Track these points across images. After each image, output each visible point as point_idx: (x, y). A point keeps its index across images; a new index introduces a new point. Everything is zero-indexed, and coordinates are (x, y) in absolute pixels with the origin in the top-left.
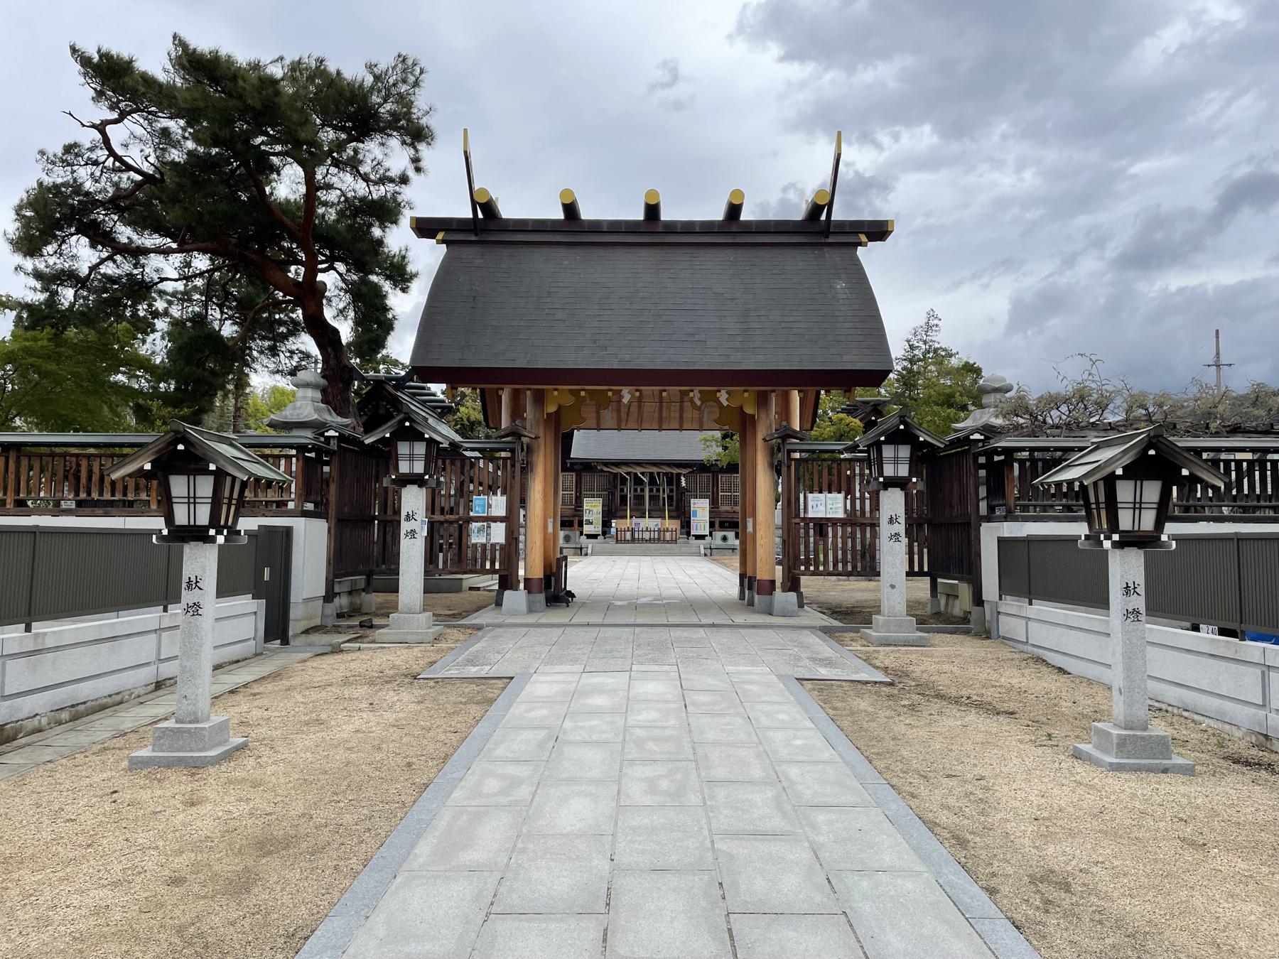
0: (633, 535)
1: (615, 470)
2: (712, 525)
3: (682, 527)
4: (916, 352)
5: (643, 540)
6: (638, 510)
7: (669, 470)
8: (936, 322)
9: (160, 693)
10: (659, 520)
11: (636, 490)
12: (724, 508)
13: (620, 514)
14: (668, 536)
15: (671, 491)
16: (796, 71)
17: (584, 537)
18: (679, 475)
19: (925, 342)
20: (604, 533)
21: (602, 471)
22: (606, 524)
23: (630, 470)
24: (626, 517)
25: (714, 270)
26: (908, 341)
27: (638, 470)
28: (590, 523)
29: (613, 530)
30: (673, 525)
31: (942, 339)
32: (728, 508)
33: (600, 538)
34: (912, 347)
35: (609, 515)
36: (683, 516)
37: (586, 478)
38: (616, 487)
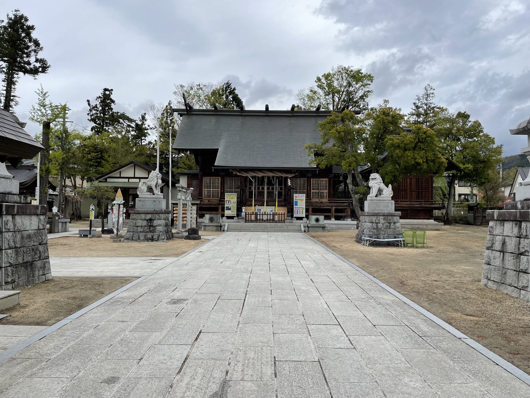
1: (245, 175)
2: (307, 210)
3: (288, 212)
4: (421, 109)
5: (263, 221)
7: (280, 174)
8: (432, 91)
10: (273, 207)
11: (258, 188)
12: (314, 200)
15: (281, 189)
16: (342, 26)
18: (286, 178)
19: (426, 105)
20: (238, 215)
21: (236, 176)
22: (239, 210)
23: (254, 174)
26: (415, 104)
27: (260, 175)
28: (229, 209)
29: (243, 214)
30: (283, 210)
31: (436, 102)
32: (317, 200)
33: (236, 218)
34: (418, 107)
35: (241, 204)
36: (288, 203)
37: (228, 181)
38: (246, 186)
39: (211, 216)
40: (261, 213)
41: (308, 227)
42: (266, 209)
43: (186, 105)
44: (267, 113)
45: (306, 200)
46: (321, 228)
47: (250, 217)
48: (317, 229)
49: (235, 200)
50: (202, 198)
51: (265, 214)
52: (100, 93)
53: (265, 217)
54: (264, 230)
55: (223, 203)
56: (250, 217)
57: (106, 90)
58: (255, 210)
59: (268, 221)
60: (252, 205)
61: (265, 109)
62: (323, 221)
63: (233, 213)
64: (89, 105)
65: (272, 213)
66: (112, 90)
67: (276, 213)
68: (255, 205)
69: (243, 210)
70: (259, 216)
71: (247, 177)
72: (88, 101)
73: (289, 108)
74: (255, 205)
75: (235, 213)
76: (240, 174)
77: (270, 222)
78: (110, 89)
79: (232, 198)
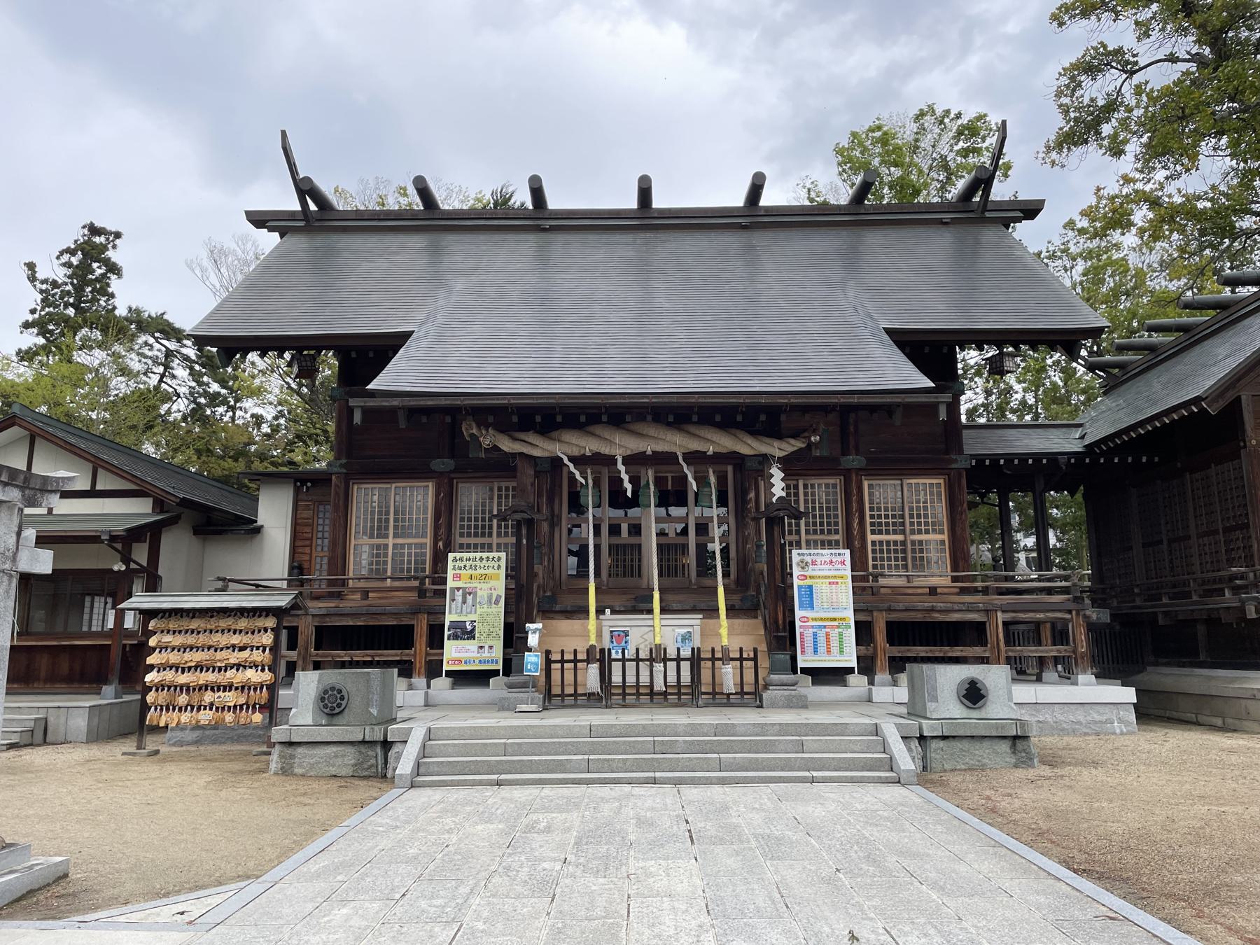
0: (605, 676)
1: (541, 447)
2: (863, 632)
6: (623, 591)
9: (37, 757)
10: (693, 622)
12: (892, 579)
13: (568, 602)
14: (728, 676)
17: (442, 683)
22: (514, 639)
23: (589, 445)
24: (583, 612)
25: (602, 268)
28: (464, 632)
29: (533, 661)
30: (728, 633)
35: (522, 604)
39: (333, 677)
41: (922, 738)
42: (666, 630)
43: (305, 189)
44: (645, 219)
45: (854, 578)
46: (1004, 747)
47: (569, 677)
48: (983, 752)
49: (499, 585)
50: (344, 583)
52: (73, 235)
53: (661, 677)
54: (656, 766)
55: (436, 601)
56: (569, 677)
57: (94, 230)
58: (599, 635)
60: (587, 612)
61: (632, 203)
62: (1010, 697)
63: (486, 654)
64: (32, 279)
65: (686, 653)
66: (118, 235)
67: (725, 650)
68: (600, 611)
69: (533, 640)
70: (616, 668)
71: (556, 462)
72: (31, 266)
73: (737, 199)
75: (498, 653)
76: (517, 447)
77: (679, 704)
78: (111, 227)
79: (484, 578)
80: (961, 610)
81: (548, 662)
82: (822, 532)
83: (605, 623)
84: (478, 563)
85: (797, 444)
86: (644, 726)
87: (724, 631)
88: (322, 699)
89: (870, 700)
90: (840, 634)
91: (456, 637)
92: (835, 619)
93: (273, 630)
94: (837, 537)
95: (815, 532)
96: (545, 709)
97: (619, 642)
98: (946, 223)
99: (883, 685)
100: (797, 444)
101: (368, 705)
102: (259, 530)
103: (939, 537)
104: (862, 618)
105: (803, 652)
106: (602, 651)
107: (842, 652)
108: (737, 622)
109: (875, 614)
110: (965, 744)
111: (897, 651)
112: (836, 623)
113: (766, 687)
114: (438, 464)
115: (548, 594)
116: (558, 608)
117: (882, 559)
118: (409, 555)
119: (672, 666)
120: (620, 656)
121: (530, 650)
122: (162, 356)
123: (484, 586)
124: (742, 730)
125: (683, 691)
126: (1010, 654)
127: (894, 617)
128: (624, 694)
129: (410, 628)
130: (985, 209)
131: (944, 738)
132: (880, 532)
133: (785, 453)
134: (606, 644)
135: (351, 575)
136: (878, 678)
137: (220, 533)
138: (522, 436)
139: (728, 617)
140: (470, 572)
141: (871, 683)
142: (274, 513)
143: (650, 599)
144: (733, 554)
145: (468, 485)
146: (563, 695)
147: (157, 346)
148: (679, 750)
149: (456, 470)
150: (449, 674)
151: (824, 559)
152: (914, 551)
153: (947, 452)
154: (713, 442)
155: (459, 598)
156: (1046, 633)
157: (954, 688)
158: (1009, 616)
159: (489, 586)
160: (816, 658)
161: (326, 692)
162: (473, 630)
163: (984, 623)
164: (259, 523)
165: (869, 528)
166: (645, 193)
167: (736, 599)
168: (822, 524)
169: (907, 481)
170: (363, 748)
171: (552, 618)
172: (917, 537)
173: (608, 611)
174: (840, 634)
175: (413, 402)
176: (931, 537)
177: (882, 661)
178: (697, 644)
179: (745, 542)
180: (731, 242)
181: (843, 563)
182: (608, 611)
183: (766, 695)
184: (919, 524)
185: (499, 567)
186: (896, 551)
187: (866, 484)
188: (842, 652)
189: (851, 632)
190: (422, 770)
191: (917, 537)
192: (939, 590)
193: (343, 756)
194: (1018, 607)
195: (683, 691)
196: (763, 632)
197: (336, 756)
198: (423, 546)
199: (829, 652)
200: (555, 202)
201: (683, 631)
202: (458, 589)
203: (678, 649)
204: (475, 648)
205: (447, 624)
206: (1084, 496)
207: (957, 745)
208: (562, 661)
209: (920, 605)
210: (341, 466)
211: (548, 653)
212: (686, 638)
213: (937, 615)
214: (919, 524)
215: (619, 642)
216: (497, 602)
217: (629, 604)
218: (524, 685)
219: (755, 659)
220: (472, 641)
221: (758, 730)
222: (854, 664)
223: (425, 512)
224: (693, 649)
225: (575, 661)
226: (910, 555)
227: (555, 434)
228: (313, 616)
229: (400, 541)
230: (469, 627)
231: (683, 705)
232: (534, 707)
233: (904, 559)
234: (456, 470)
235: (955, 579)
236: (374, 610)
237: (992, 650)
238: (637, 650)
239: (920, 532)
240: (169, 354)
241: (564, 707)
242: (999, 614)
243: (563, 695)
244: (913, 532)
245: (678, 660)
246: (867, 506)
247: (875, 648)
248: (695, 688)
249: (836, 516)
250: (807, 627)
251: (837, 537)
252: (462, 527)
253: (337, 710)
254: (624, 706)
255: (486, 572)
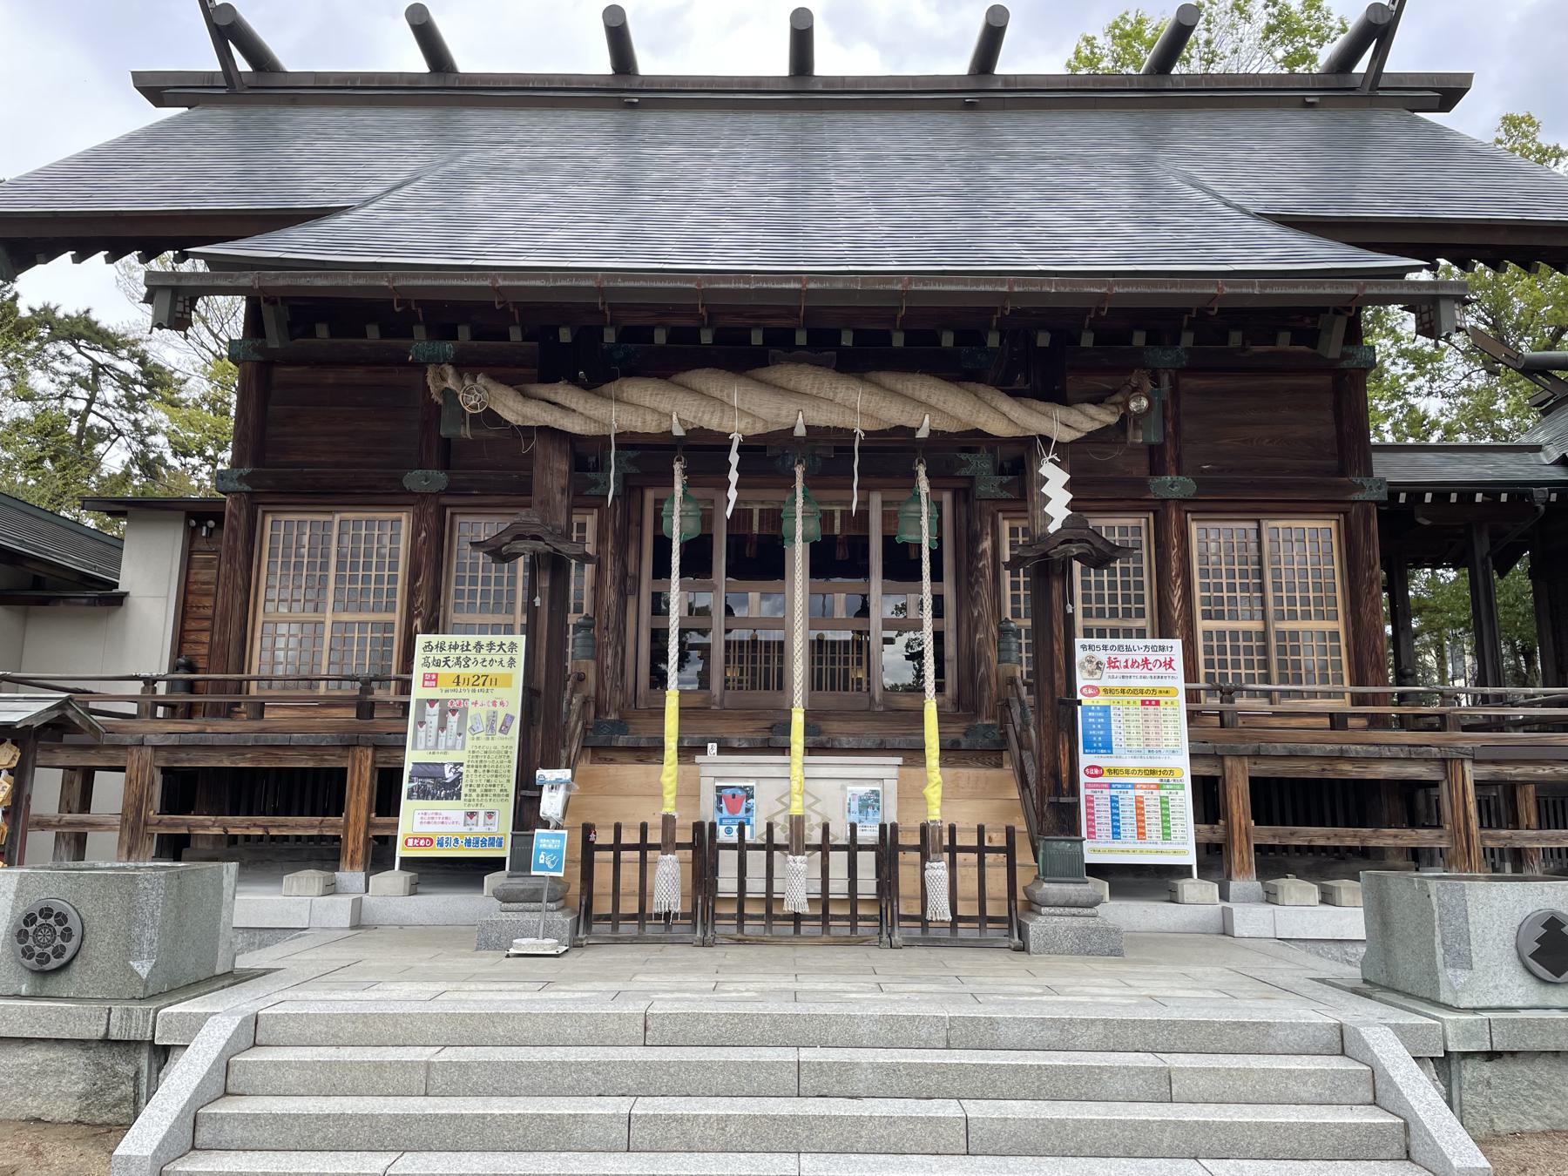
5: (768, 922)
10: (883, 771)
18: (1017, 460)
28: (440, 785)
29: (552, 849)
30: (941, 795)
36: (1024, 730)
40: (755, 834)
42: (819, 791)
43: (228, 31)
47: (630, 874)
50: (240, 687)
51: (797, 844)
56: (630, 874)
58: (688, 793)
59: (830, 921)
61: (779, 65)
63: (480, 828)
65: (869, 834)
68: (688, 752)
70: (727, 860)
73: (959, 65)
74: (688, 752)
75: (503, 825)
79: (482, 681)
80: (1389, 759)
81: (589, 848)
82: (1114, 613)
83: (705, 771)
84: (472, 654)
85: (1104, 417)
86: (776, 1021)
87: (934, 793)
88: (22, 935)
89: (1226, 930)
90: (1164, 801)
91: (422, 793)
92: (1153, 772)
93: (11, 772)
94: (1140, 623)
95: (1101, 614)
96: (576, 945)
97: (733, 810)
98: (1311, 105)
99: (1246, 899)
100: (1104, 417)
101: (128, 954)
102: (119, 600)
103: (1328, 626)
104: (1206, 770)
105: (414, 747)
106: (698, 827)
107: (1166, 836)
108: (968, 774)
109: (1228, 763)
110: (1541, 1071)
111: (1269, 835)
112: (1155, 780)
113: (1033, 906)
114: (415, 480)
115: (613, 717)
116: (622, 741)
117: (1223, 664)
118: (362, 640)
119: (839, 860)
120: (734, 838)
121: (546, 824)
122: (86, 373)
123: (479, 697)
124: (1013, 1034)
125: (861, 911)
126: (1489, 844)
127: (1265, 769)
128: (741, 917)
129: (338, 778)
130: (1375, 86)
131: (1492, 1055)
132: (1220, 616)
133: (1097, 426)
134: (707, 813)
135: (254, 673)
136: (1235, 886)
137: (45, 602)
138: (544, 390)
139: (944, 762)
140: (456, 670)
141: (1224, 896)
142: (150, 574)
143: (786, 729)
144: (950, 650)
145: (471, 519)
146: (615, 918)
147: (78, 358)
148: (860, 1088)
149: (448, 492)
150: (407, 863)
151: (1131, 656)
152: (1282, 650)
153: (1342, 472)
154: (930, 408)
155: (433, 713)
156: (1528, 806)
157: (1509, 936)
158: (1486, 771)
159: (490, 697)
160: (1117, 845)
161: (30, 919)
162: (457, 781)
163: (1435, 784)
164: (121, 589)
165: (1198, 609)
166: (802, 41)
167: (956, 730)
168: (1113, 599)
169: (1268, 525)
170: (105, 1057)
171: (612, 761)
172: (1287, 625)
173: (712, 748)
174: (1164, 801)
175: (282, 280)
176: (1314, 625)
177: (1243, 855)
178: (891, 817)
179: (974, 626)
180: (954, 125)
181: (1169, 664)
182: (712, 748)
183: (1036, 927)
184: (1292, 601)
185: (512, 662)
186: (1249, 650)
187: (1194, 527)
188: (1166, 836)
189: (1186, 796)
190: (204, 1136)
191: (1287, 625)
192: (1327, 722)
193: (60, 1073)
194: (1497, 755)
195: (861, 911)
196: (1015, 794)
197: (42, 1073)
198: (388, 626)
199: (1141, 834)
200: (648, 64)
201: (863, 789)
202: (432, 702)
203: (853, 827)
204: (460, 816)
205: (408, 769)
206: (1532, 574)
207: (1522, 1073)
208: (617, 847)
209: (1317, 749)
210: (241, 478)
211: (588, 829)
212: (869, 803)
213: (1347, 767)
214: (1292, 601)
215: (733, 810)
216: (505, 728)
217: (759, 736)
218: (533, 896)
219: (1009, 850)
220: (453, 803)
221: (1051, 1035)
222: (1190, 859)
223: (393, 566)
224: (883, 827)
225: (643, 847)
226: (1274, 658)
227: (611, 388)
228: (156, 748)
229: (346, 617)
230: (449, 776)
231: (862, 942)
232: (548, 945)
233: (1265, 664)
234: (448, 492)
235: (1358, 700)
236: (270, 738)
237: (1453, 836)
238: (770, 827)
239: (1293, 616)
240: (97, 369)
241: (617, 941)
242: (1468, 766)
243: (615, 918)
244: (1281, 617)
245: (853, 848)
246: (1196, 567)
247: (1228, 828)
248: (876, 905)
249: (1139, 586)
250: (1100, 786)
251: (1140, 623)
252: (459, 594)
253: (54, 963)
254: (740, 942)
255: (488, 670)
